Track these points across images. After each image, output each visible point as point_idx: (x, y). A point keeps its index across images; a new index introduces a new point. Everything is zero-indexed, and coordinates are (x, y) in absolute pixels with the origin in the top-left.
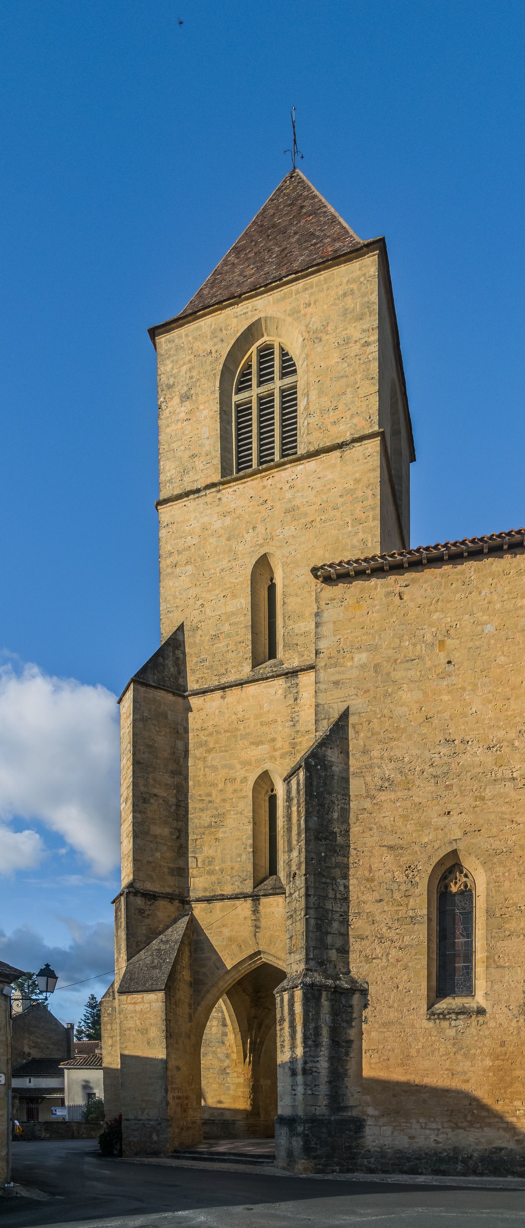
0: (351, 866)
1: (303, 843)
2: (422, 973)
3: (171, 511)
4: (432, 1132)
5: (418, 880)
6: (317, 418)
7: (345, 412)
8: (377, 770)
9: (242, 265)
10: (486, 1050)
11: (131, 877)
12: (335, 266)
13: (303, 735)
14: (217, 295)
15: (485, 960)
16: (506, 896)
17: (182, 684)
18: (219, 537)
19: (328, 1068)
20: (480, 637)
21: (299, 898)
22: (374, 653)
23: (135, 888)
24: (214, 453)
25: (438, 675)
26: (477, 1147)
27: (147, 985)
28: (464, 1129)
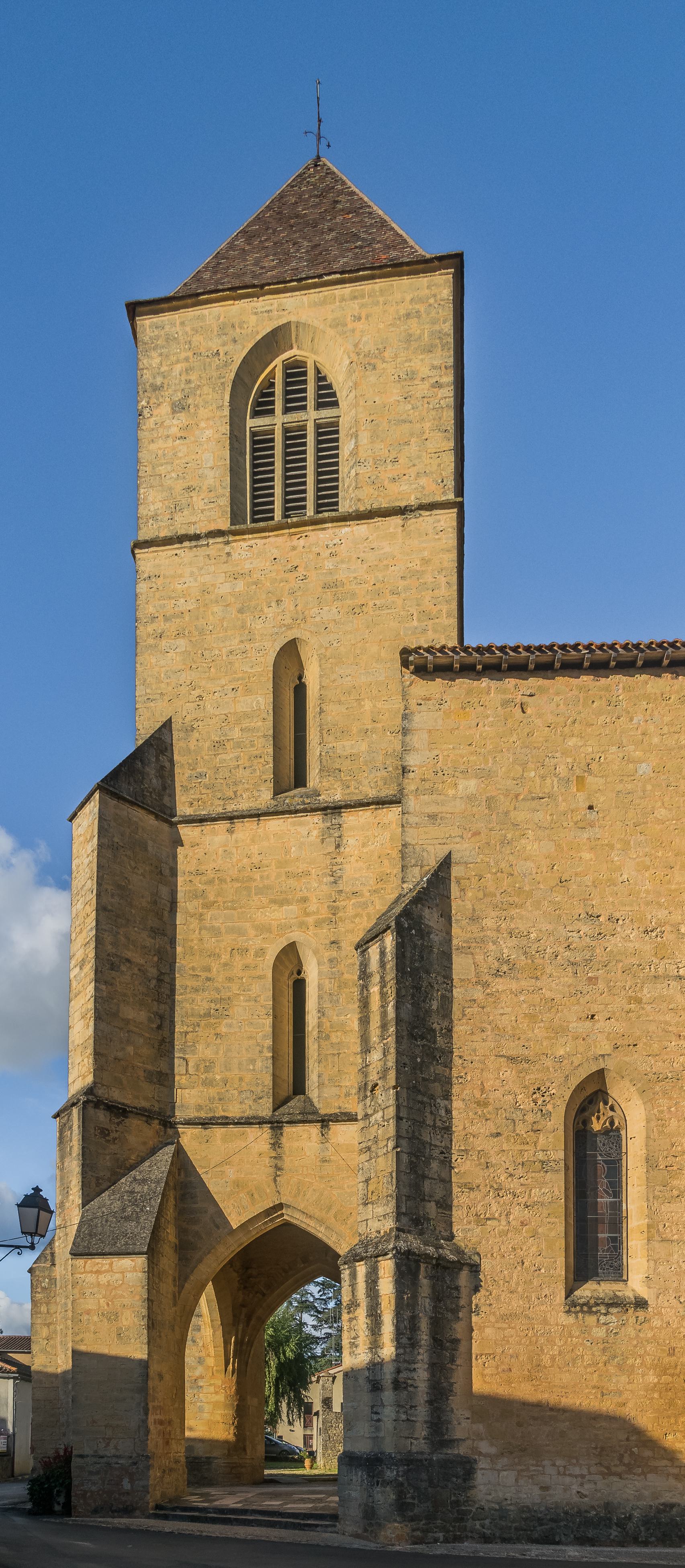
0: (454, 1080)
1: (391, 1040)
2: (557, 1244)
3: (155, 559)
4: (575, 1480)
5: (551, 1109)
6: (370, 469)
7: (409, 468)
8: (491, 947)
9: (257, 253)
10: (648, 1359)
11: (90, 1079)
12: (394, 276)
13: (348, 898)
14: (224, 283)
15: (646, 1230)
16: (673, 1141)
17: (168, 805)
18: (227, 605)
19: (428, 1380)
20: (633, 778)
21: (384, 1121)
22: (486, 782)
23: (96, 1097)
24: (220, 491)
25: (576, 823)
26: (638, 1503)
27: (118, 1245)
28: (620, 1475)
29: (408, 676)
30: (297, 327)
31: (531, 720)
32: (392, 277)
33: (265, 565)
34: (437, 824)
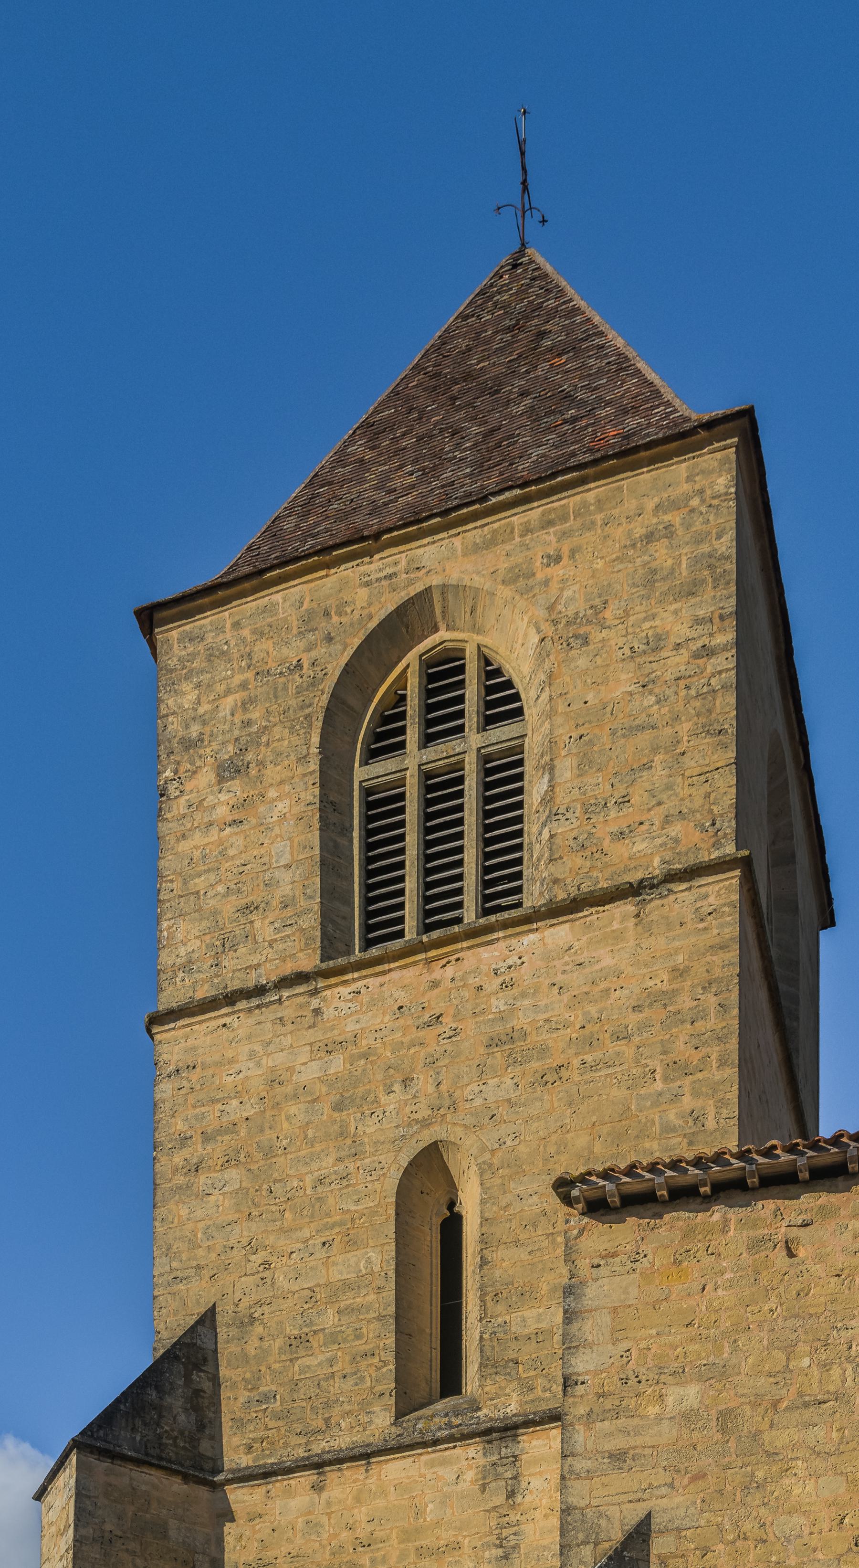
6: (576, 823)
7: (649, 810)
9: (384, 464)
17: (209, 1454)
18: (314, 1101)
22: (718, 1386)
24: (303, 903)
29: (577, 1220)
30: (443, 593)
31: (803, 1268)
32: (619, 473)
33: (382, 1022)
34: (626, 1468)
